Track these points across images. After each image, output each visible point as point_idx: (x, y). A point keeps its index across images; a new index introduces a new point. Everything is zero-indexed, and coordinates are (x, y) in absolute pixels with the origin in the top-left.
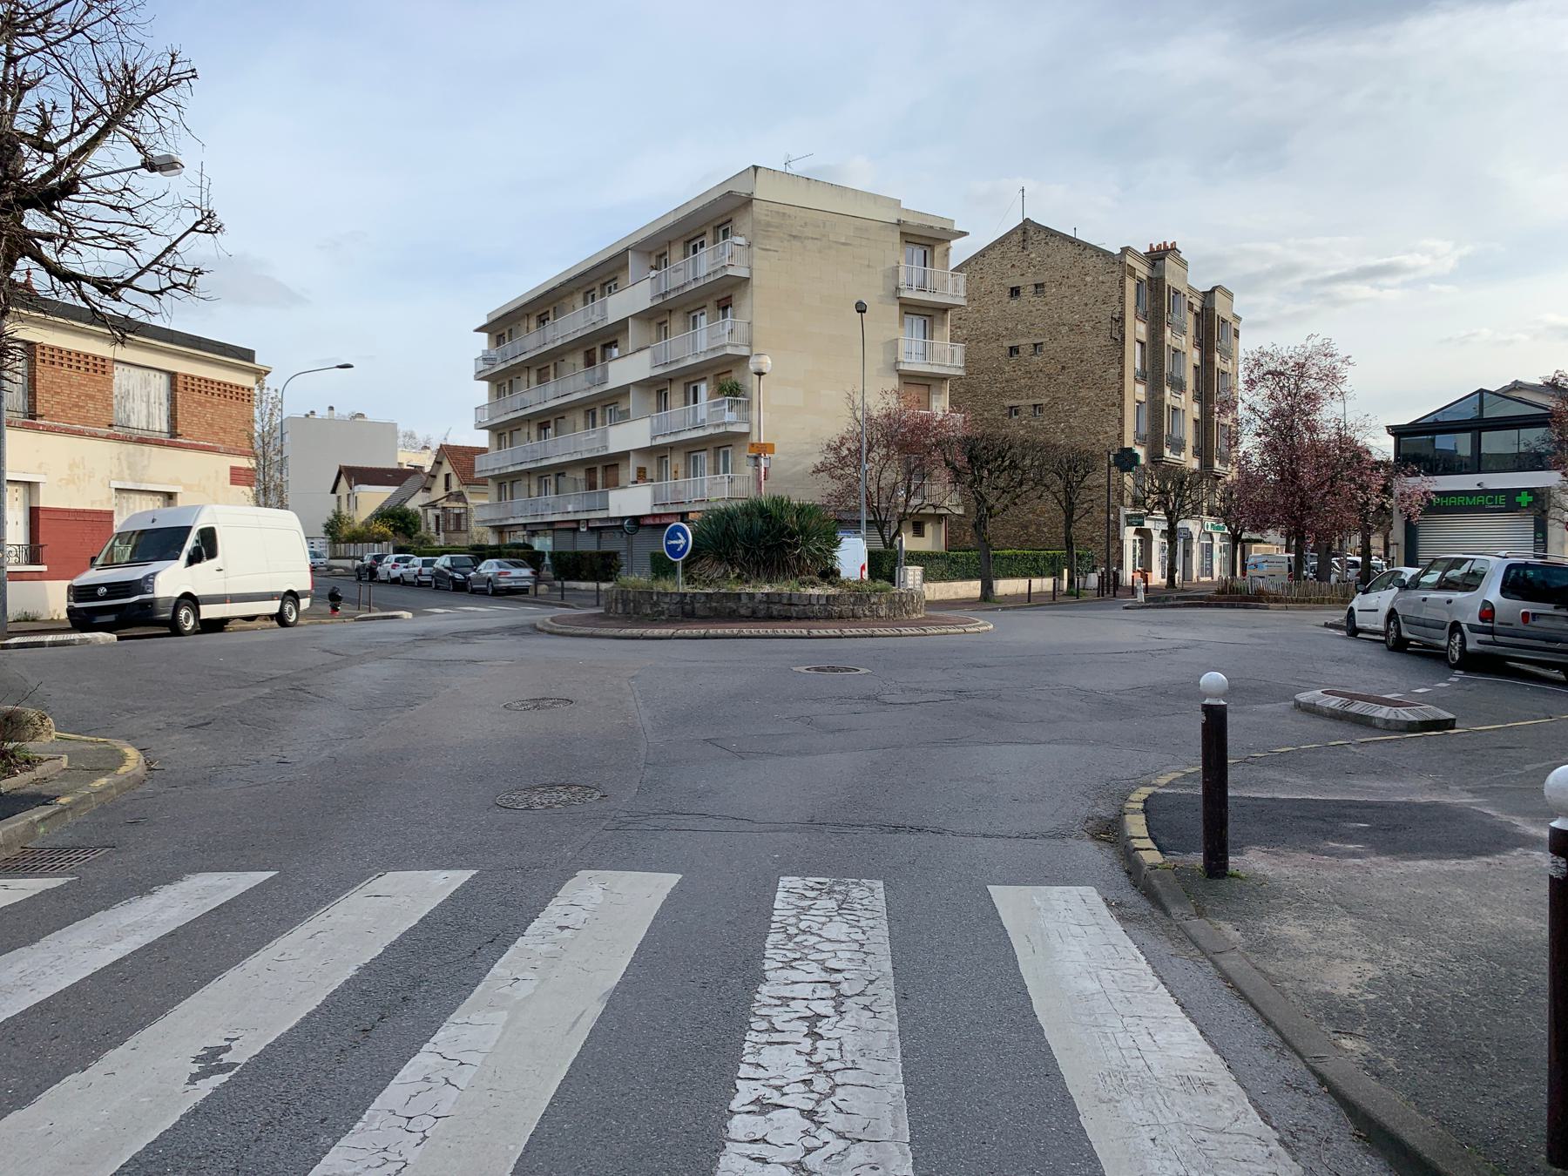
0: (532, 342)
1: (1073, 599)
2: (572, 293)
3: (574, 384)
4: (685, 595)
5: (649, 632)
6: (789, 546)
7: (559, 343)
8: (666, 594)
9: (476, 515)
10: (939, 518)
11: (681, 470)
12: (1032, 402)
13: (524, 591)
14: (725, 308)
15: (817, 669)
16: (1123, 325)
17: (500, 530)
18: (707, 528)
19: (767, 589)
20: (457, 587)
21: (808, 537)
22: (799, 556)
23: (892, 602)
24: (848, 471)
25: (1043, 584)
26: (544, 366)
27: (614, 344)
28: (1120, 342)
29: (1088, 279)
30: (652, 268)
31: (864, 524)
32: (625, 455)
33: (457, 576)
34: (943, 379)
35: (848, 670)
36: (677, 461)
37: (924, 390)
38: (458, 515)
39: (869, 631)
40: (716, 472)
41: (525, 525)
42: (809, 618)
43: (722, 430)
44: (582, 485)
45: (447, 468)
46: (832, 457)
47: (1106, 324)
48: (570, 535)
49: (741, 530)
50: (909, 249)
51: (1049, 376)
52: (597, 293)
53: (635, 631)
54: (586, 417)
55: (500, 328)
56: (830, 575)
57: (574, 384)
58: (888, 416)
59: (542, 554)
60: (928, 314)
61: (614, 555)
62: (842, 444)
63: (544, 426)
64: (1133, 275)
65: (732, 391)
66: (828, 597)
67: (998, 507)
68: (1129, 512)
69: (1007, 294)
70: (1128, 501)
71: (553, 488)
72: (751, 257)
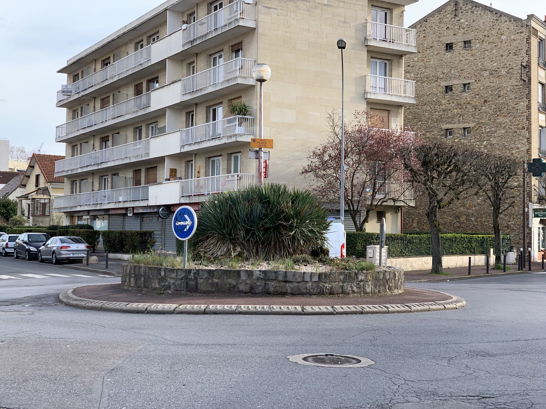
0: (97, 78)
1: (501, 272)
2: (126, 44)
3: (126, 108)
4: (189, 271)
5: (154, 306)
6: (285, 227)
7: (116, 79)
8: (172, 271)
9: (56, 204)
10: (397, 209)
11: (202, 171)
12: (462, 126)
13: (78, 261)
14: (237, 51)
15: (317, 359)
16: (530, 71)
17: (71, 215)
18: (212, 211)
19: (264, 266)
20: (32, 257)
21: (303, 220)
22: (293, 237)
23: (376, 279)
24: (330, 171)
25: (479, 260)
26: (105, 95)
27: (155, 80)
28: (527, 83)
29: (503, 37)
30: (184, 22)
31: (342, 212)
32: (161, 160)
33: (32, 249)
34: (399, 106)
35: (348, 360)
36: (199, 164)
37: (384, 114)
38: (44, 204)
39: (359, 308)
40: (229, 171)
41: (88, 211)
42: (302, 294)
43: (233, 140)
44: (130, 182)
45: (37, 170)
46: (316, 161)
47: (517, 69)
48: (120, 219)
49: (243, 214)
50: (374, 11)
51: (475, 107)
52: (145, 43)
53: (141, 306)
54: (135, 132)
55: (75, 69)
56: (320, 254)
57: (126, 108)
58: (360, 131)
59: (97, 233)
60: (385, 58)
61: (150, 234)
62: (324, 152)
63: (104, 140)
64: (536, 35)
65: (241, 112)
66: (320, 275)
67: (446, 199)
68: (537, 206)
69: (443, 47)
70: (535, 198)
71: (109, 184)
72: (257, 13)
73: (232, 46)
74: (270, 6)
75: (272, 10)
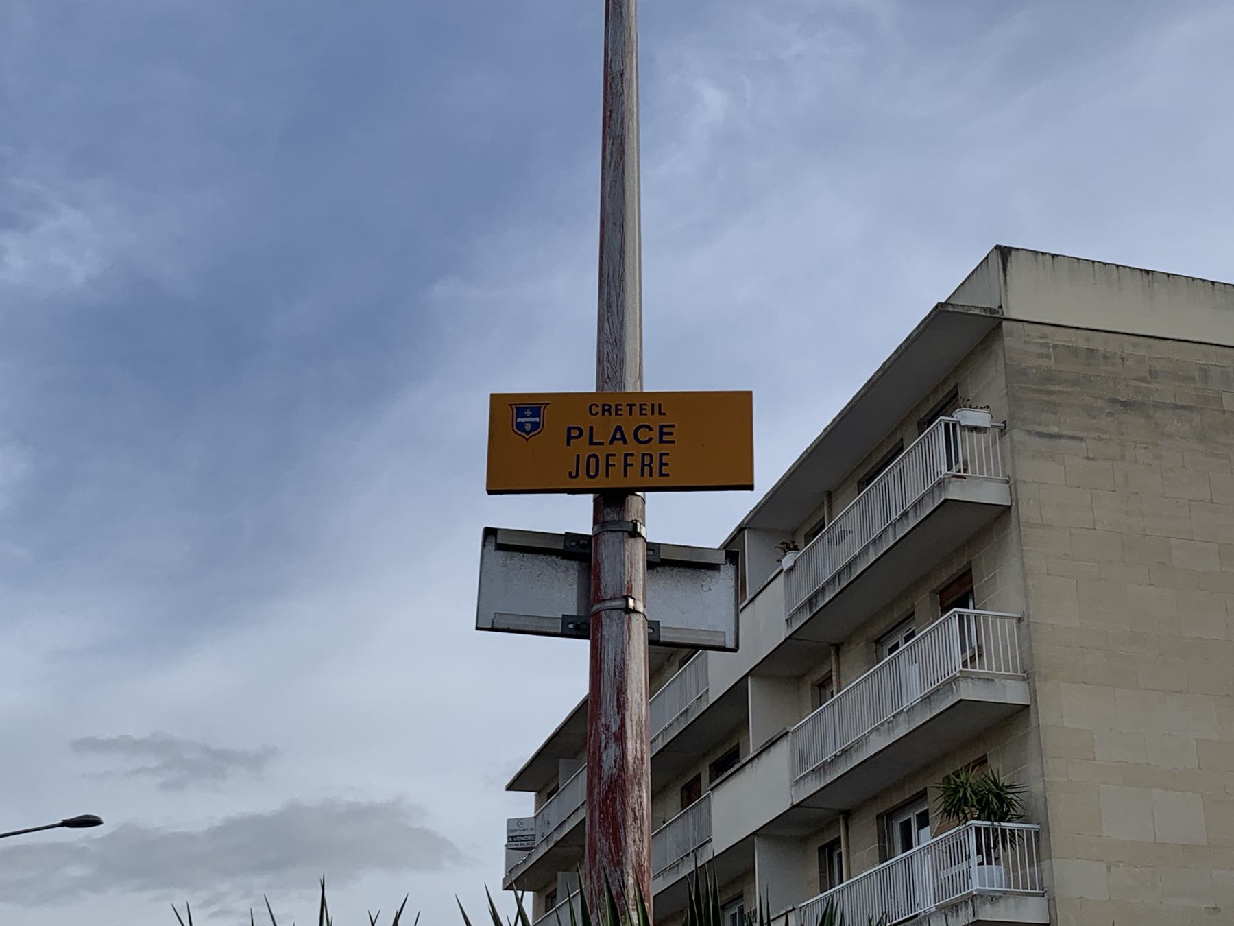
73: (941, 593)
74: (1055, 430)
75: (1063, 441)
